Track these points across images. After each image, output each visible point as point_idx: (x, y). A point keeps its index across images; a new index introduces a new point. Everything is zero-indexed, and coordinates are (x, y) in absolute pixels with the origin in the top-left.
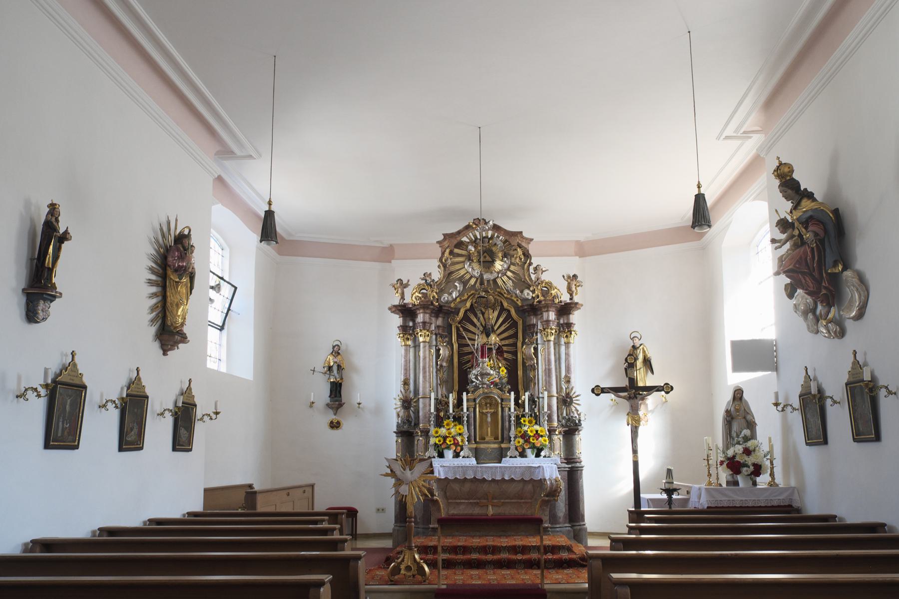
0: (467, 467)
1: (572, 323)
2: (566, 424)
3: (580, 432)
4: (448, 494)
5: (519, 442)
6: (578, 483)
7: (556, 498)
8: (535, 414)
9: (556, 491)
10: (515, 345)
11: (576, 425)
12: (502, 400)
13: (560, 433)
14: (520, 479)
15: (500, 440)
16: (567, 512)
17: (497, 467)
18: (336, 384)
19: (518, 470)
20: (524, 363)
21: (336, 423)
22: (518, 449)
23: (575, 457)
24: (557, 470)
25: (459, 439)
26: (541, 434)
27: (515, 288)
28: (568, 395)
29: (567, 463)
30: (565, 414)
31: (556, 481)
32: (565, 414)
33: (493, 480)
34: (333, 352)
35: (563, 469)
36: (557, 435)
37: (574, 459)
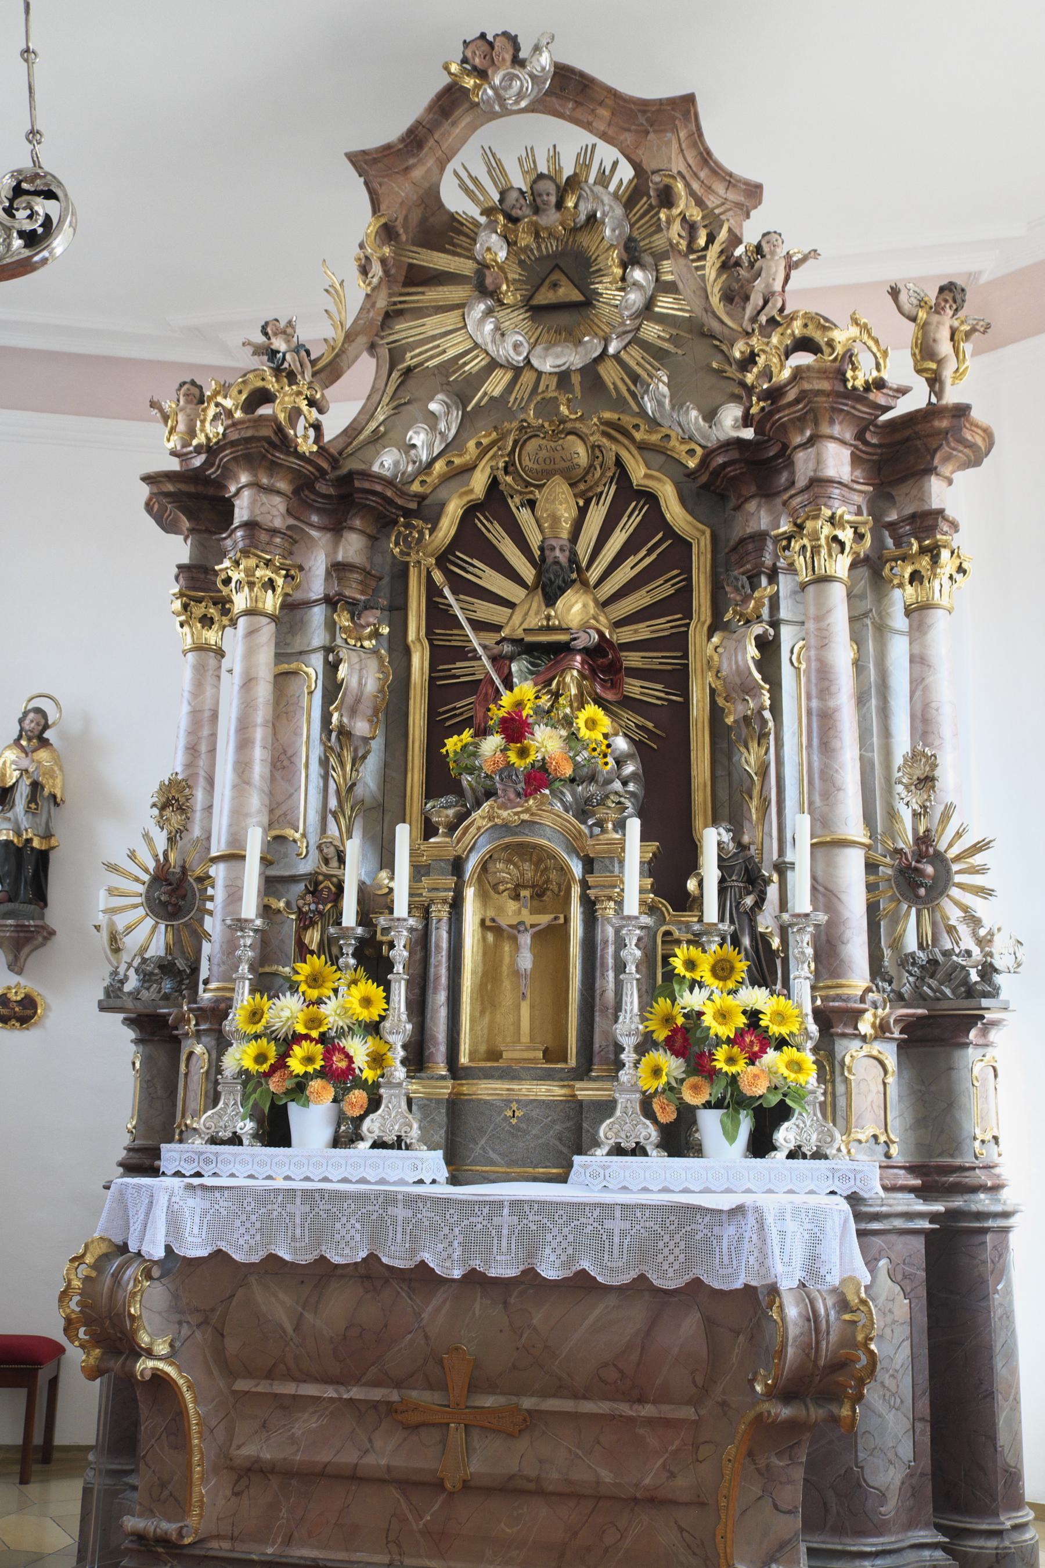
0: (338, 1197)
1: (940, 512)
2: (916, 988)
3: (993, 1035)
4: (232, 1345)
5: (656, 1072)
6: (986, 1297)
7: (845, 1412)
8: (761, 941)
9: (840, 1365)
10: (678, 642)
11: (970, 992)
12: (589, 864)
13: (882, 1029)
14: (625, 1279)
15: (572, 1062)
16: (926, 1463)
17: (545, 1207)
18: (19, 851)
19: (617, 1225)
20: (716, 713)
21: (19, 1003)
22: (656, 1107)
23: (968, 1160)
24: (852, 1226)
25: (359, 1049)
26: (775, 1030)
27: (678, 404)
28: (924, 840)
29: (922, 1192)
30: (911, 944)
31: (844, 1305)
32: (911, 944)
33: (474, 1279)
34: (20, 737)
35: (899, 1223)
36: (864, 1038)
37: (962, 1169)
